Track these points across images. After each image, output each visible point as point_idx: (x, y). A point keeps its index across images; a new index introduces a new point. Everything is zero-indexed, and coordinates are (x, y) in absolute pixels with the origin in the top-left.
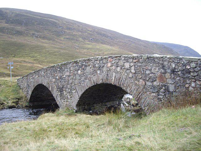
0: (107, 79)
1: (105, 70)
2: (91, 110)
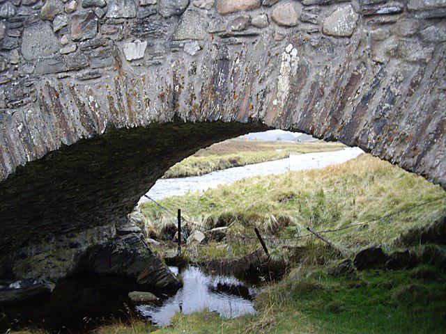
0: (215, 89)
1: (202, 33)
2: (14, 281)
